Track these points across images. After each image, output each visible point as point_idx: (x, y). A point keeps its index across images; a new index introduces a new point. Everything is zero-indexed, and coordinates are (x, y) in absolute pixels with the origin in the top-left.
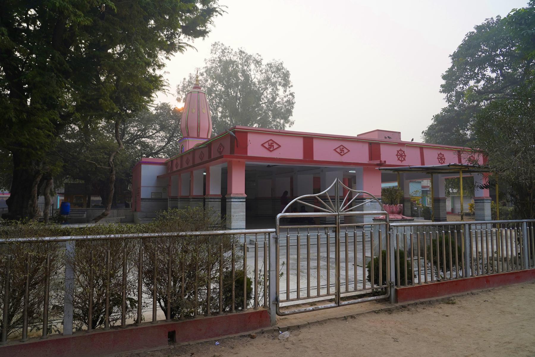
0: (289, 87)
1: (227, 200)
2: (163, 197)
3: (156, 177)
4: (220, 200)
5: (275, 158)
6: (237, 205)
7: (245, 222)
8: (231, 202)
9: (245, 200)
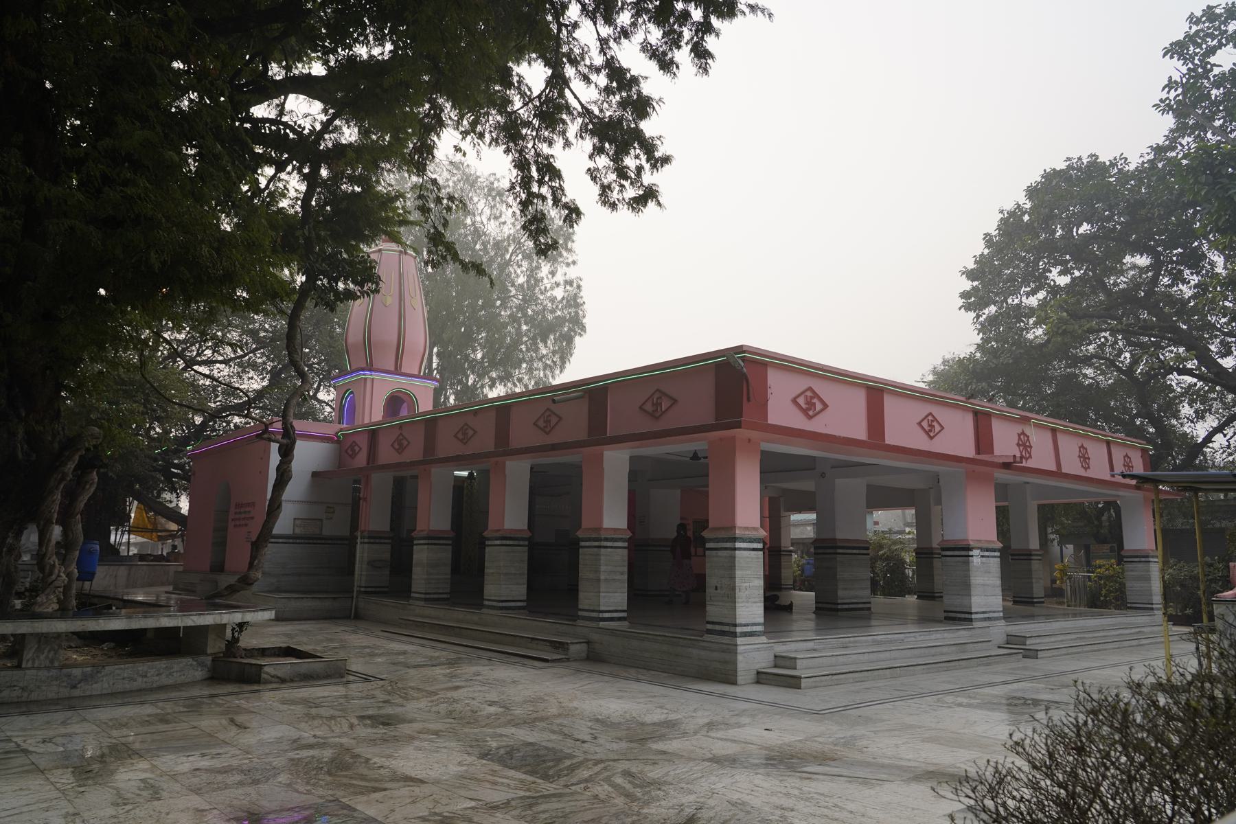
0: (568, 265)
1: (415, 542)
2: (326, 532)
6: (748, 557)
8: (735, 549)
9: (527, 543)
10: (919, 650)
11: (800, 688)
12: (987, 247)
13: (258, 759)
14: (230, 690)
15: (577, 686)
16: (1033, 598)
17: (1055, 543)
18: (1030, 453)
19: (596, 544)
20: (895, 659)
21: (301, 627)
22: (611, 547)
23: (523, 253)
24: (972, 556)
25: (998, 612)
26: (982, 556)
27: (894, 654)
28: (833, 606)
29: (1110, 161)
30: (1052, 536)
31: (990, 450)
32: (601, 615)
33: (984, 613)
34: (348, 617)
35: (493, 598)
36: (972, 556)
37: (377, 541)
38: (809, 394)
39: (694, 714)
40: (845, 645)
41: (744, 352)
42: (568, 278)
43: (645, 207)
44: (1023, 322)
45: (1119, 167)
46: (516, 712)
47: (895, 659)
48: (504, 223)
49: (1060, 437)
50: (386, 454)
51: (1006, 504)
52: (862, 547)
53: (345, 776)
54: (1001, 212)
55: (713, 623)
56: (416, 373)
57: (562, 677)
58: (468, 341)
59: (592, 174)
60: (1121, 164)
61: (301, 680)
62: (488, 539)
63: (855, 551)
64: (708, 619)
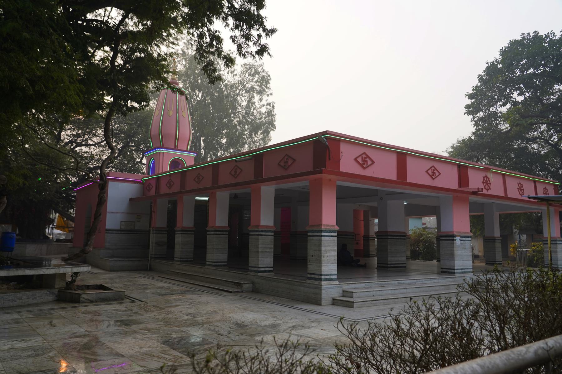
0: (268, 95)
1: (176, 233)
3: (129, 199)
4: (273, 234)
5: (376, 178)
6: (328, 240)
7: (337, 264)
8: (321, 236)
9: (336, 234)
10: (423, 288)
11: (353, 308)
12: (480, 82)
13: (48, 343)
14: (62, 306)
15: (238, 305)
16: (496, 262)
17: (517, 234)
18: (489, 187)
19: (257, 233)
20: (409, 293)
21: (118, 275)
22: (265, 235)
23: (246, 90)
24: (456, 240)
25: (470, 269)
26: (461, 240)
27: (408, 290)
28: (386, 265)
29: (545, 35)
30: (515, 231)
31: (467, 185)
32: (259, 269)
33: (462, 269)
34: (146, 270)
35: (211, 261)
36: (456, 240)
37: (160, 232)
38: (364, 156)
39: (289, 321)
40: (382, 286)
41: (327, 134)
42: (268, 102)
43: (263, 56)
44: (498, 120)
45: (550, 38)
46: (198, 319)
47: (409, 293)
48: (236, 75)
49: (507, 178)
50: (164, 189)
51: (483, 213)
52: (403, 236)
53: (85, 353)
54: (487, 63)
55: (311, 274)
56: (186, 150)
57: (233, 301)
58: (218, 133)
59: (233, 39)
60: (552, 36)
61: (101, 302)
62: (208, 231)
63: (398, 238)
64: (309, 272)
